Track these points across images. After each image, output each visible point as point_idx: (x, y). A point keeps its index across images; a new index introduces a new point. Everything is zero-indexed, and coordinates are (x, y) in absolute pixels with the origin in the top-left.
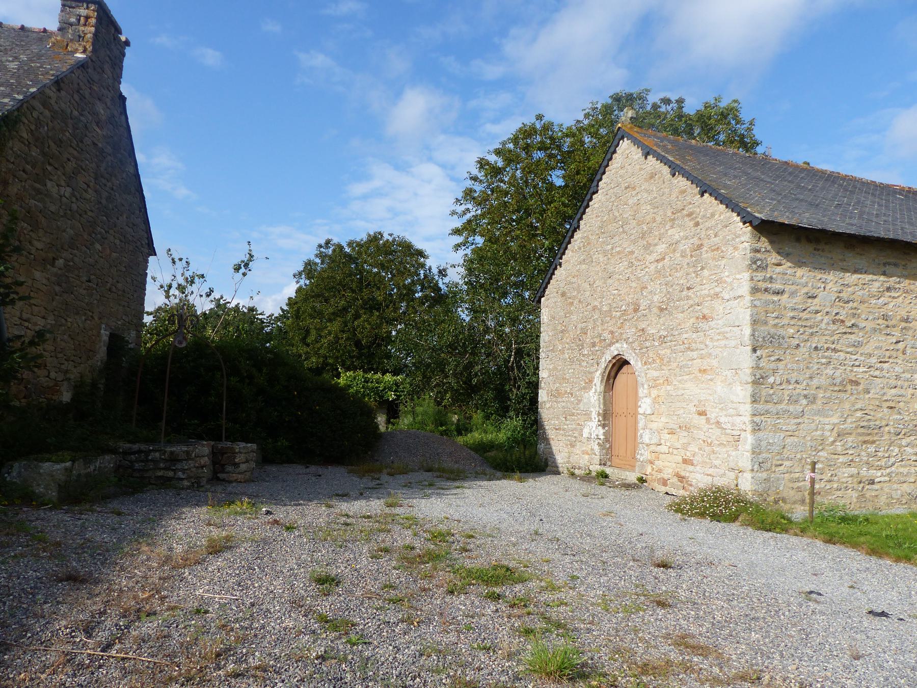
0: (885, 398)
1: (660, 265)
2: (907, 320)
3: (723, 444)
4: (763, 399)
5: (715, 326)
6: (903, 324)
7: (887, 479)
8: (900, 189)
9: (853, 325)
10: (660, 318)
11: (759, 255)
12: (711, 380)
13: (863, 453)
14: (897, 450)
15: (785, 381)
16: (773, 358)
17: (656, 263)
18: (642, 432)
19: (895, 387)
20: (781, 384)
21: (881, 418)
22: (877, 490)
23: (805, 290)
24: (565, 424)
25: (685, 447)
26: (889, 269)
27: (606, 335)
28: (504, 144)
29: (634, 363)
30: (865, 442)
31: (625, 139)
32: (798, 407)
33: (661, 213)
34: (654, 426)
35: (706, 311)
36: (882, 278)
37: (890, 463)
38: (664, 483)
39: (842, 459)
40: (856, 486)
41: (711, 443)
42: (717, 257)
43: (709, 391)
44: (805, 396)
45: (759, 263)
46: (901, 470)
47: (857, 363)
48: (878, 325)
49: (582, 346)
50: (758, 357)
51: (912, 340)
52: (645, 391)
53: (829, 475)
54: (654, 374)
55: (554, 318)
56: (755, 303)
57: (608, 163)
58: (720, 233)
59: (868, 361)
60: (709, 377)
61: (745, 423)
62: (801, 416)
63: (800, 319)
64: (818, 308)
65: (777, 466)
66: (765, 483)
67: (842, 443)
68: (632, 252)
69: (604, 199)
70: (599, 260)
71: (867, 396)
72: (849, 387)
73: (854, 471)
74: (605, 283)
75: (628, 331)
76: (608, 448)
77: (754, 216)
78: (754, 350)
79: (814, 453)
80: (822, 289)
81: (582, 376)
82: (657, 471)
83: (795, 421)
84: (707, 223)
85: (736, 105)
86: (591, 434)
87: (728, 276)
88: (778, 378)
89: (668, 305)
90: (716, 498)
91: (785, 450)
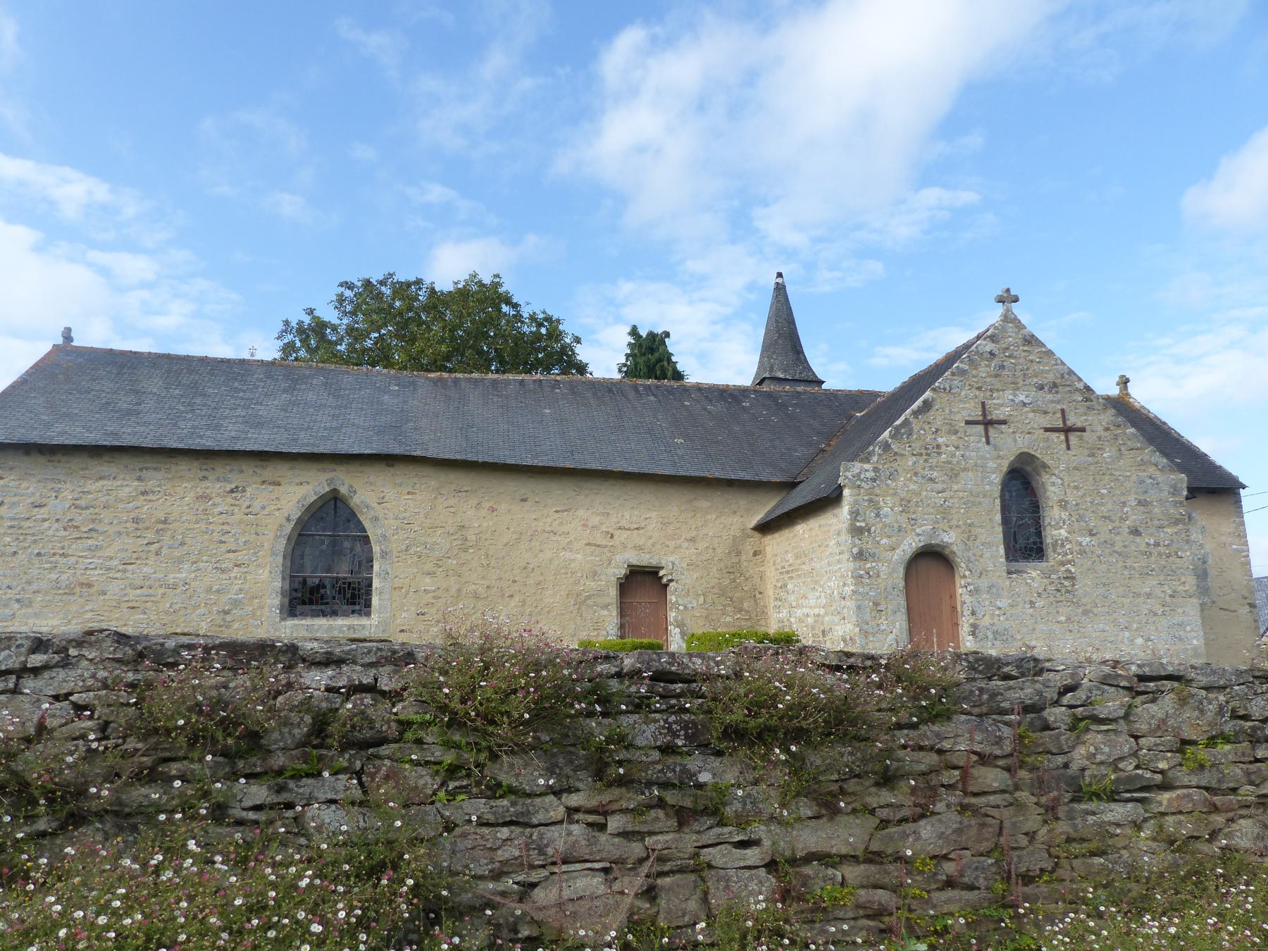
0: (127, 598)
6: (161, 526)
64: (45, 516)
72: (78, 589)
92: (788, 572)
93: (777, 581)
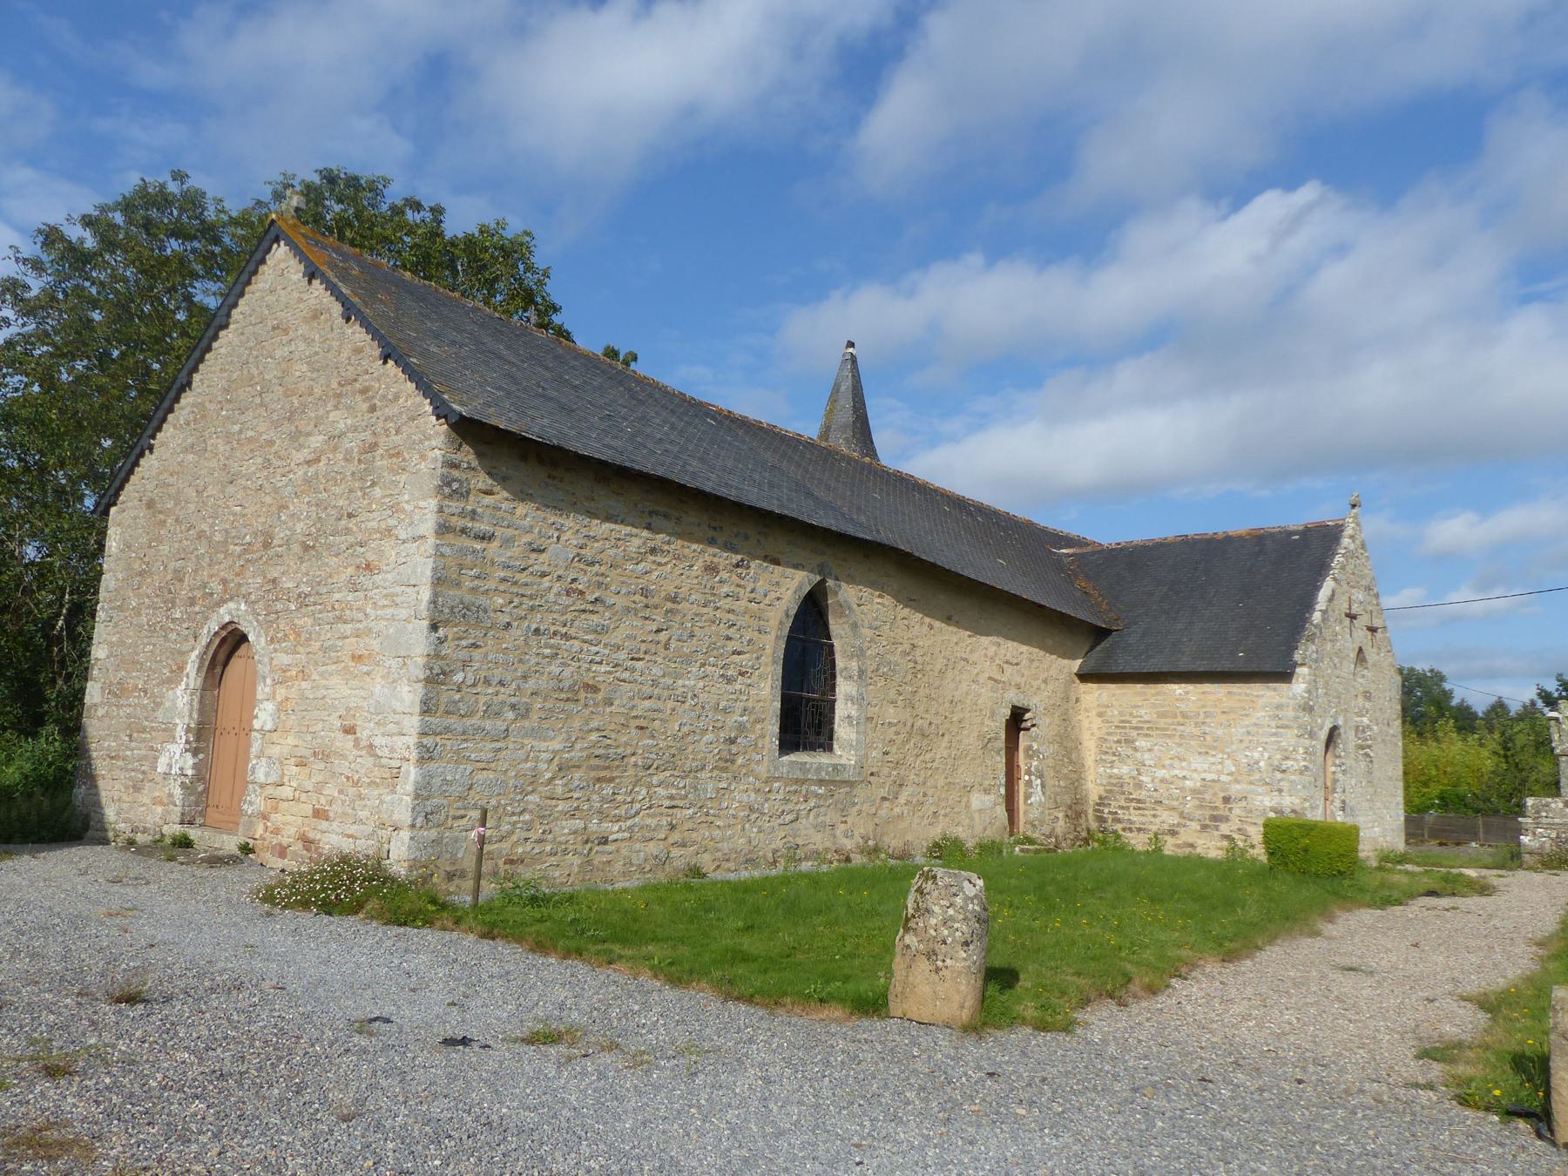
0: (634, 713)
1: (311, 471)
2: (674, 600)
3: (375, 783)
4: (442, 708)
5: (381, 583)
6: (669, 605)
7: (627, 835)
8: (715, 412)
9: (596, 600)
10: (302, 562)
11: (456, 473)
12: (368, 674)
13: (595, 797)
14: (644, 792)
15: (482, 680)
16: (464, 643)
17: (306, 466)
18: (254, 762)
19: (650, 698)
20: (474, 685)
21: (626, 744)
22: (610, 853)
23: (527, 538)
24: (128, 748)
25: (319, 788)
26: (656, 521)
27: (216, 587)
28: (104, 209)
29: (254, 638)
30: (599, 780)
31: (282, 243)
32: (499, 723)
33: (322, 381)
34: (275, 751)
35: (371, 557)
36: (645, 533)
37: (633, 812)
38: (282, 852)
39: (562, 806)
40: (580, 848)
41: (358, 781)
42: (396, 467)
43: (363, 693)
44: (513, 707)
45: (455, 486)
46: (649, 821)
47: (598, 659)
48: (634, 602)
49: (173, 603)
50: (439, 638)
51: (679, 629)
52: (267, 690)
53: (541, 831)
54: (284, 659)
55: (129, 547)
56: (443, 550)
57: (250, 279)
58: (404, 428)
59: (614, 656)
60: (365, 669)
61: (408, 747)
62: (504, 738)
63: (516, 583)
64: (545, 568)
65: (455, 818)
66: (432, 847)
67: (565, 780)
68: (271, 443)
69: (236, 341)
70: (216, 448)
71: (608, 710)
72: (582, 695)
73: (579, 824)
74: (223, 492)
75: (250, 581)
76: (202, 793)
77: (451, 408)
78: (434, 627)
79: (519, 797)
80: (555, 539)
81: (167, 658)
82: (272, 832)
83: (493, 746)
84: (387, 410)
85: (528, 239)
86: (171, 767)
87: (408, 502)
88: (470, 675)
89: (316, 538)
90: (337, 875)
91: (472, 792)
92: (1136, 728)
93: (1108, 734)
